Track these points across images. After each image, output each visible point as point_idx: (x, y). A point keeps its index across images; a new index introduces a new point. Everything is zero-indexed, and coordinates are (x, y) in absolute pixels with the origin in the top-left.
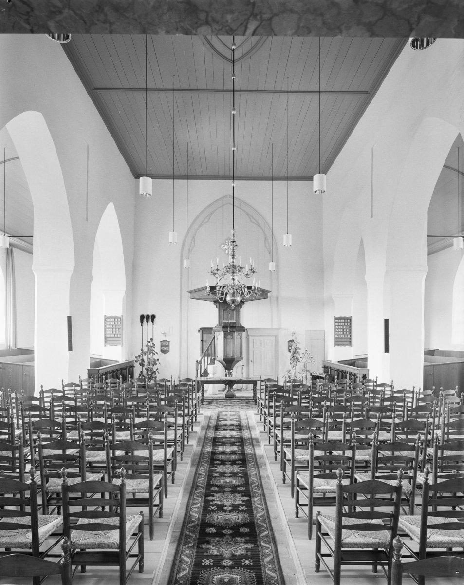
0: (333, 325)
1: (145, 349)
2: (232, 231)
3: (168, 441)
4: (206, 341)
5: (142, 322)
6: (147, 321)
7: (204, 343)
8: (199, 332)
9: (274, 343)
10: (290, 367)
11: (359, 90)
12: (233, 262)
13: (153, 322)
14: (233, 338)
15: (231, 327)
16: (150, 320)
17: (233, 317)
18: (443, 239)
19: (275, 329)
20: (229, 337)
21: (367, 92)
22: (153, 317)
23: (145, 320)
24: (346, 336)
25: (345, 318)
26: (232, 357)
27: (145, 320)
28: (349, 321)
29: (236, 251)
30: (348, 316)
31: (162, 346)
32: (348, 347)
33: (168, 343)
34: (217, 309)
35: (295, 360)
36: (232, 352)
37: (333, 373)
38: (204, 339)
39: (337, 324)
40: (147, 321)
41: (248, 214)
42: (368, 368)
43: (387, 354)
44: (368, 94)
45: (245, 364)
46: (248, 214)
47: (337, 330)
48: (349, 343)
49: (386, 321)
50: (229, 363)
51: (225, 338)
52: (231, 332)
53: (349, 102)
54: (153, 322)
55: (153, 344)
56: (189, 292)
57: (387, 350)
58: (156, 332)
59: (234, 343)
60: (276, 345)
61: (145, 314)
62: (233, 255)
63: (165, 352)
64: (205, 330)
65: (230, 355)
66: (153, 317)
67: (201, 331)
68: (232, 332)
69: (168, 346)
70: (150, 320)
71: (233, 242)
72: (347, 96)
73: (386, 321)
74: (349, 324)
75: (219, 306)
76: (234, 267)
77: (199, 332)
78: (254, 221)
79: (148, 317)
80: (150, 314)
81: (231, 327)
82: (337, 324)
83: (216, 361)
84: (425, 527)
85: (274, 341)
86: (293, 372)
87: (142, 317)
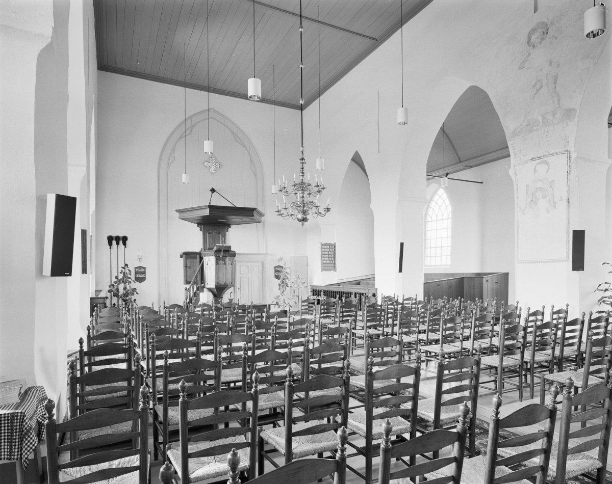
0: (320, 251)
1: (121, 276)
2: (301, 149)
3: (222, 383)
4: (189, 268)
5: (110, 244)
6: (118, 244)
7: (188, 269)
8: (181, 256)
9: (261, 270)
10: (278, 293)
11: (371, 36)
12: (303, 180)
13: (124, 244)
14: (225, 264)
15: (225, 251)
16: (121, 242)
17: (220, 240)
18: (433, 178)
19: (262, 254)
20: (221, 262)
21: (376, 39)
22: (125, 239)
23: (114, 242)
24: (331, 262)
25: (330, 245)
26: (225, 283)
27: (114, 242)
28: (333, 247)
29: (305, 169)
30: (332, 243)
31: (136, 273)
32: (332, 272)
33: (143, 270)
34: (201, 233)
35: (284, 284)
36: (225, 279)
37: (461, 289)
38: (188, 266)
39: (323, 250)
40: (118, 244)
41: (233, 133)
42: (376, 287)
43: (400, 273)
44: (377, 42)
45: (233, 292)
46: (233, 133)
47: (323, 256)
48: (333, 268)
49: (402, 244)
50: (218, 291)
51: (217, 263)
52: (223, 256)
53: (363, 43)
54: (124, 244)
55: (129, 270)
56: (177, 211)
57: (400, 270)
58: (131, 256)
59: (226, 269)
60: (263, 270)
61: (114, 235)
62: (303, 173)
63: (140, 280)
64: (188, 256)
65: (222, 282)
66: (125, 239)
67: (184, 256)
68: (224, 257)
69: (144, 273)
70: (121, 242)
71: (302, 159)
72: (359, 39)
73: (402, 244)
74: (333, 250)
75: (204, 230)
76: (302, 183)
77: (181, 256)
78: (238, 140)
79: (118, 239)
80: (121, 235)
81: (225, 251)
82: (323, 250)
83: (205, 289)
84: (290, 436)
85: (261, 267)
86: (282, 298)
87: (110, 239)
